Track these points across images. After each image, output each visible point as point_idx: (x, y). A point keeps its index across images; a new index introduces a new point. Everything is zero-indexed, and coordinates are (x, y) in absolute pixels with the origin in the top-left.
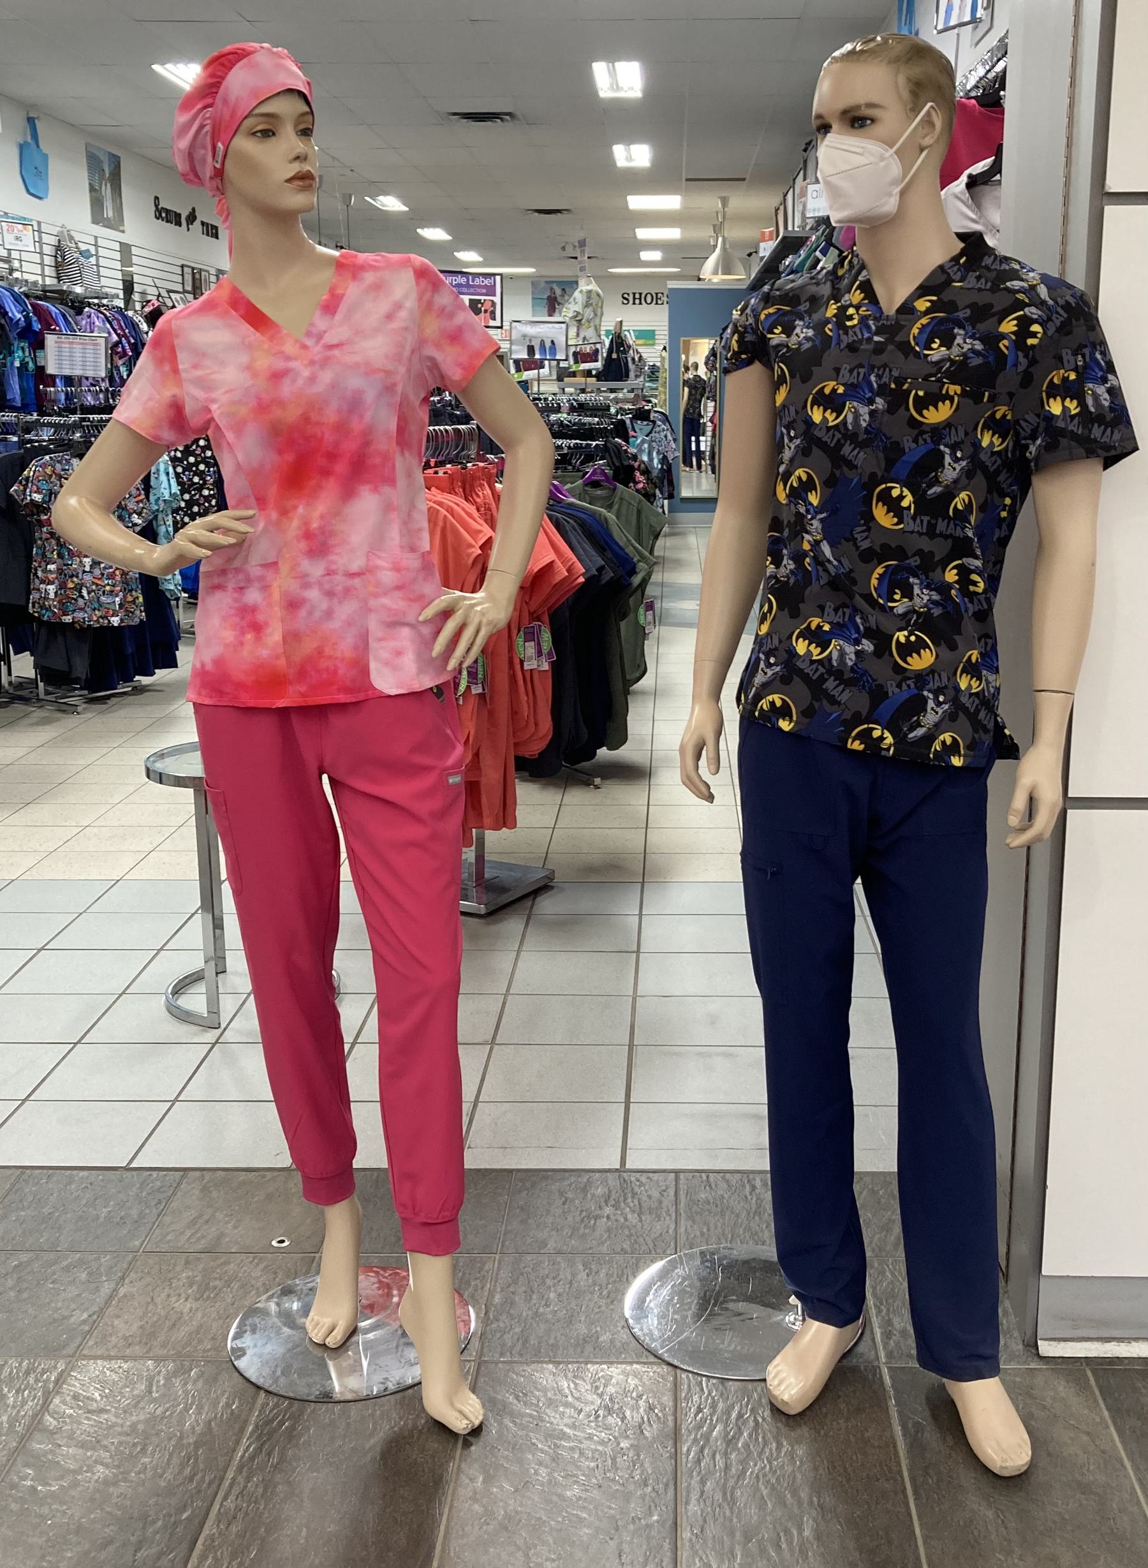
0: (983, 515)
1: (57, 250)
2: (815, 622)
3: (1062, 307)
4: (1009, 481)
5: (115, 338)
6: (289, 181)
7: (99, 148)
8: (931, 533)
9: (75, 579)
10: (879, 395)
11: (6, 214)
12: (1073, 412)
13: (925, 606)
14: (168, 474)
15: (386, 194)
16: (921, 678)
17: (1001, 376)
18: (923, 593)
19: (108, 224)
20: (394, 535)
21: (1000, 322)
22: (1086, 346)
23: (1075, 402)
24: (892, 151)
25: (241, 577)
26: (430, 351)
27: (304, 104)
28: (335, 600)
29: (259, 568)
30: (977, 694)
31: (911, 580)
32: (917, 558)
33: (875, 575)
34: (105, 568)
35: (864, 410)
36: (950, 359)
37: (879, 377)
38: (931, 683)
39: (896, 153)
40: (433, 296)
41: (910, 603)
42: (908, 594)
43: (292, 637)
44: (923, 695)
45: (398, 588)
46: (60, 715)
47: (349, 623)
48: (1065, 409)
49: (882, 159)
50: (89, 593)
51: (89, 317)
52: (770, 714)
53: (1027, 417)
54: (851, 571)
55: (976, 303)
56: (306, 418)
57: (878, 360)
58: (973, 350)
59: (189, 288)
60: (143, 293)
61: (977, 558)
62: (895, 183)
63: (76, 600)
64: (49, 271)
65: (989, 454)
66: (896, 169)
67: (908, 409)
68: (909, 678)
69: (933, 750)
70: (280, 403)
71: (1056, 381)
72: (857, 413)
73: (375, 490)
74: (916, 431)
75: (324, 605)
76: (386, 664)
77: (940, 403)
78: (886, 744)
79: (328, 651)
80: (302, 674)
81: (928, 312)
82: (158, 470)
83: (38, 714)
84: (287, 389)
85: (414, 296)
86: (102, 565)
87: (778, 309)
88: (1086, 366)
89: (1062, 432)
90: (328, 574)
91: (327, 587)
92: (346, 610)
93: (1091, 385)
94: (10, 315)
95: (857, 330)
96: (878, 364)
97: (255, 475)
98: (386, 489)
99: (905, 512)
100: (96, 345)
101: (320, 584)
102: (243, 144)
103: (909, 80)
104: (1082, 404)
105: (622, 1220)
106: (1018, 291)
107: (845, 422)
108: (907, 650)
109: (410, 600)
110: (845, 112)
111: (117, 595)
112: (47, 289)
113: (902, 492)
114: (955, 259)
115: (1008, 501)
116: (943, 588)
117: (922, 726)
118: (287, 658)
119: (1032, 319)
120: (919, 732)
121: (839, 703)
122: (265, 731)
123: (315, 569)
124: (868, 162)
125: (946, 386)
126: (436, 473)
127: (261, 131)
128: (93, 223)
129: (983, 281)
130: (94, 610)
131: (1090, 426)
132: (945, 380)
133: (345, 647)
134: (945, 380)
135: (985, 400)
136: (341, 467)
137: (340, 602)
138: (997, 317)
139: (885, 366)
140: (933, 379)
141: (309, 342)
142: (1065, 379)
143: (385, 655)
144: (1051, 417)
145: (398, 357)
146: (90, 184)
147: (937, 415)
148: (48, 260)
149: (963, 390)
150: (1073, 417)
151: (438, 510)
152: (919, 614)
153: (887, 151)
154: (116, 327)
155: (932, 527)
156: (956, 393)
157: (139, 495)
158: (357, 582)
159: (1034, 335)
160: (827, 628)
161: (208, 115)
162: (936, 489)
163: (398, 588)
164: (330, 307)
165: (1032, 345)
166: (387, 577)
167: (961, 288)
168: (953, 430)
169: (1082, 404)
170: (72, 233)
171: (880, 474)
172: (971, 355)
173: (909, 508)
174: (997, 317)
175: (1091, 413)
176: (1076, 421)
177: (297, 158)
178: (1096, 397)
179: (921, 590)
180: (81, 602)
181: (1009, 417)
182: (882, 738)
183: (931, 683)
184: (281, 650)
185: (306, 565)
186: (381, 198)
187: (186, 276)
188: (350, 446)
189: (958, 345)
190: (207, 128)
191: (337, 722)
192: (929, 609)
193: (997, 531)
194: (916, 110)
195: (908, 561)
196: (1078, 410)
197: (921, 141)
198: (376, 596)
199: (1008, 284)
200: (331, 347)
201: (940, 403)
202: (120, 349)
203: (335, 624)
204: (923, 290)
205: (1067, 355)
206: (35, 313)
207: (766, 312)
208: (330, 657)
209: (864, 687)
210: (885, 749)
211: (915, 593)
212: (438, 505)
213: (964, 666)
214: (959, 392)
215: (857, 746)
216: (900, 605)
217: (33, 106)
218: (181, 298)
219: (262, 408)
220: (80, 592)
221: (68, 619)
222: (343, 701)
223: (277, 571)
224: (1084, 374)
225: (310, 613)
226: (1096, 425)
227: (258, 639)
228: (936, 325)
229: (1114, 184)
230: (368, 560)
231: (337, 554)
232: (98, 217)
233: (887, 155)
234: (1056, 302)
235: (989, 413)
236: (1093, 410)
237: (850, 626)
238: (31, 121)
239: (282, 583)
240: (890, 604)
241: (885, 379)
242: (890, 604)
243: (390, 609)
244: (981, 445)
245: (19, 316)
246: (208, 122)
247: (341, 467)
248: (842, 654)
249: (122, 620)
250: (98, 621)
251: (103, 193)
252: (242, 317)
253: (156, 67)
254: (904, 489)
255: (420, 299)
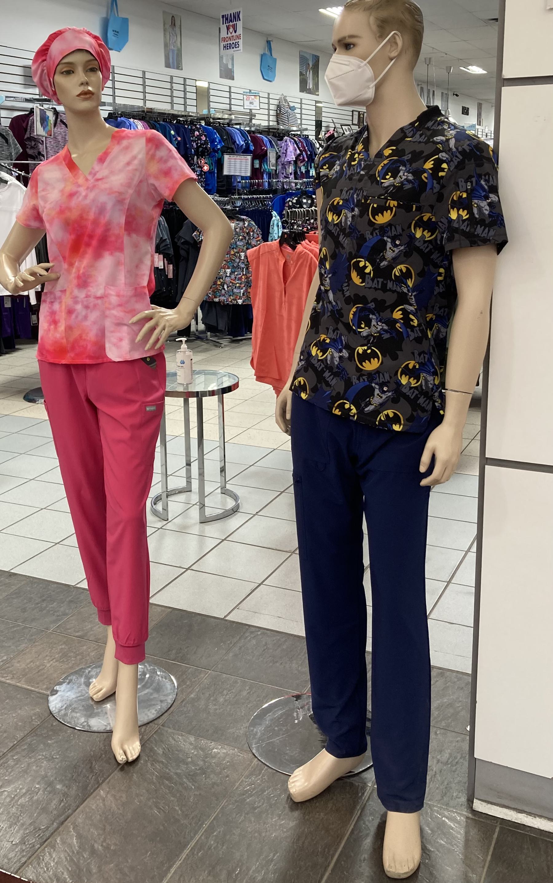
0: (421, 279)
1: (278, 107)
2: (323, 337)
3: (460, 152)
4: (441, 259)
5: (298, 152)
6: (78, 96)
7: (305, 52)
8: (384, 288)
9: (221, 280)
10: (357, 206)
11: (250, 91)
12: (464, 218)
13: (378, 332)
14: (278, 226)
15: (472, 65)
16: (371, 375)
17: (423, 195)
18: (378, 324)
19: (309, 92)
20: (122, 279)
21: (425, 162)
22: (473, 177)
23: (466, 212)
24: (365, 62)
25: (52, 296)
26: (152, 181)
27: (90, 55)
28: (89, 310)
29: (59, 292)
30: (416, 388)
31: (371, 316)
32: (373, 303)
33: (352, 312)
34: (237, 275)
35: (350, 215)
36: (394, 185)
37: (358, 195)
38: (378, 378)
39: (368, 63)
40: (155, 152)
41: (369, 330)
42: (368, 325)
43: (69, 328)
44: (372, 386)
45: (120, 305)
46: (214, 348)
47: (94, 323)
48: (459, 216)
49: (360, 67)
50: (228, 287)
51: (286, 141)
52: (299, 389)
53: (442, 220)
54: (341, 309)
55: (415, 151)
56: (81, 217)
57: (360, 185)
58: (407, 180)
59: (356, 122)
60: (328, 127)
61: (411, 305)
62: (369, 80)
63: (221, 290)
64: (272, 118)
65: (422, 242)
66: (369, 72)
67: (368, 215)
68: (364, 375)
69: (378, 419)
70: (69, 209)
71: (455, 198)
72: (347, 216)
73: (111, 254)
74: (372, 228)
75: (84, 313)
76: (115, 345)
77: (385, 212)
78: (352, 413)
79: (84, 337)
80: (73, 348)
81: (390, 155)
82: (273, 224)
83: (204, 345)
84: (74, 203)
85: (144, 151)
86: (236, 273)
87: (331, 154)
88: (473, 189)
89: (456, 230)
90: (86, 297)
91: (85, 303)
92: (94, 316)
93: (476, 201)
94: (238, 143)
95: (355, 167)
96: (359, 187)
97: (60, 245)
98: (117, 254)
99: (367, 276)
100: (247, 159)
101: (82, 302)
102: (59, 79)
103: (377, 19)
104: (470, 212)
105: (47, 658)
106: (439, 143)
107: (341, 221)
108: (365, 357)
109: (125, 312)
110: (340, 41)
111: (242, 289)
112: (270, 127)
113: (365, 264)
114: (412, 124)
115: (442, 270)
116: (391, 323)
117: (372, 405)
118: (67, 339)
119: (442, 160)
120: (370, 408)
121: (330, 386)
122: (60, 374)
123: (81, 295)
124: (352, 69)
125: (389, 201)
126: (315, 233)
127: (65, 71)
128: (300, 91)
129: (423, 136)
130: (230, 296)
131: (475, 227)
132: (389, 198)
133: (92, 335)
134: (389, 198)
135: (414, 209)
136: (94, 243)
137: (91, 312)
138: (423, 159)
139: (361, 189)
140: (383, 197)
141: (90, 177)
142: (460, 197)
143: (114, 340)
144: (450, 221)
145: (129, 185)
146: (300, 72)
147: (383, 219)
148: (272, 113)
149: (398, 203)
150: (464, 221)
151: (308, 254)
152: (374, 337)
153: (362, 62)
154: (300, 146)
155: (384, 286)
156: (394, 206)
157: (258, 237)
158: (99, 301)
159: (443, 170)
160: (328, 341)
161: (44, 65)
162: (384, 263)
163: (120, 305)
164: (102, 159)
165: (441, 176)
166: (114, 300)
167: (410, 141)
168: (393, 228)
169: (470, 212)
170: (287, 98)
171: (353, 253)
172: (406, 183)
173: (370, 273)
174: (423, 159)
175: (476, 218)
176: (466, 223)
177: (82, 84)
178: (480, 208)
179: (377, 322)
180: (223, 291)
181: (433, 220)
182: (350, 409)
183: (378, 378)
184: (64, 335)
185: (76, 292)
186: (470, 67)
187: (354, 116)
188: (99, 231)
189: (400, 176)
190: (45, 71)
191: (91, 374)
192: (381, 334)
193: (436, 288)
194: (382, 36)
195: (369, 305)
196: (467, 216)
197: (389, 54)
198: (109, 309)
199: (435, 139)
200: (98, 180)
201: (385, 212)
202: (301, 158)
203: (88, 323)
204: (390, 143)
205: (462, 183)
206: (252, 141)
207: (323, 156)
208: (85, 340)
209: (342, 377)
210: (352, 416)
211: (372, 324)
212: (310, 252)
213: (402, 370)
214: (396, 205)
215: (337, 412)
216: (364, 331)
217: (270, 35)
218: (349, 129)
219: (62, 211)
220: (223, 287)
221: (216, 300)
222: (88, 363)
223: (65, 295)
224: (472, 194)
225: (77, 317)
226: (479, 226)
227: (56, 328)
228: (392, 164)
229: (507, 73)
230: (105, 290)
231: (92, 287)
232: (303, 88)
233: (362, 64)
234: (457, 149)
235: (418, 217)
236: (477, 216)
237: (339, 341)
238: (269, 43)
239: (67, 300)
240: (359, 330)
241: (360, 197)
242: (359, 330)
243: (115, 316)
244: (415, 236)
245: (242, 143)
246: (45, 68)
247: (94, 243)
248: (332, 357)
249: (243, 302)
250: (231, 301)
251: (308, 76)
252: (66, 165)
253: (321, 10)
254: (367, 262)
255: (147, 153)
